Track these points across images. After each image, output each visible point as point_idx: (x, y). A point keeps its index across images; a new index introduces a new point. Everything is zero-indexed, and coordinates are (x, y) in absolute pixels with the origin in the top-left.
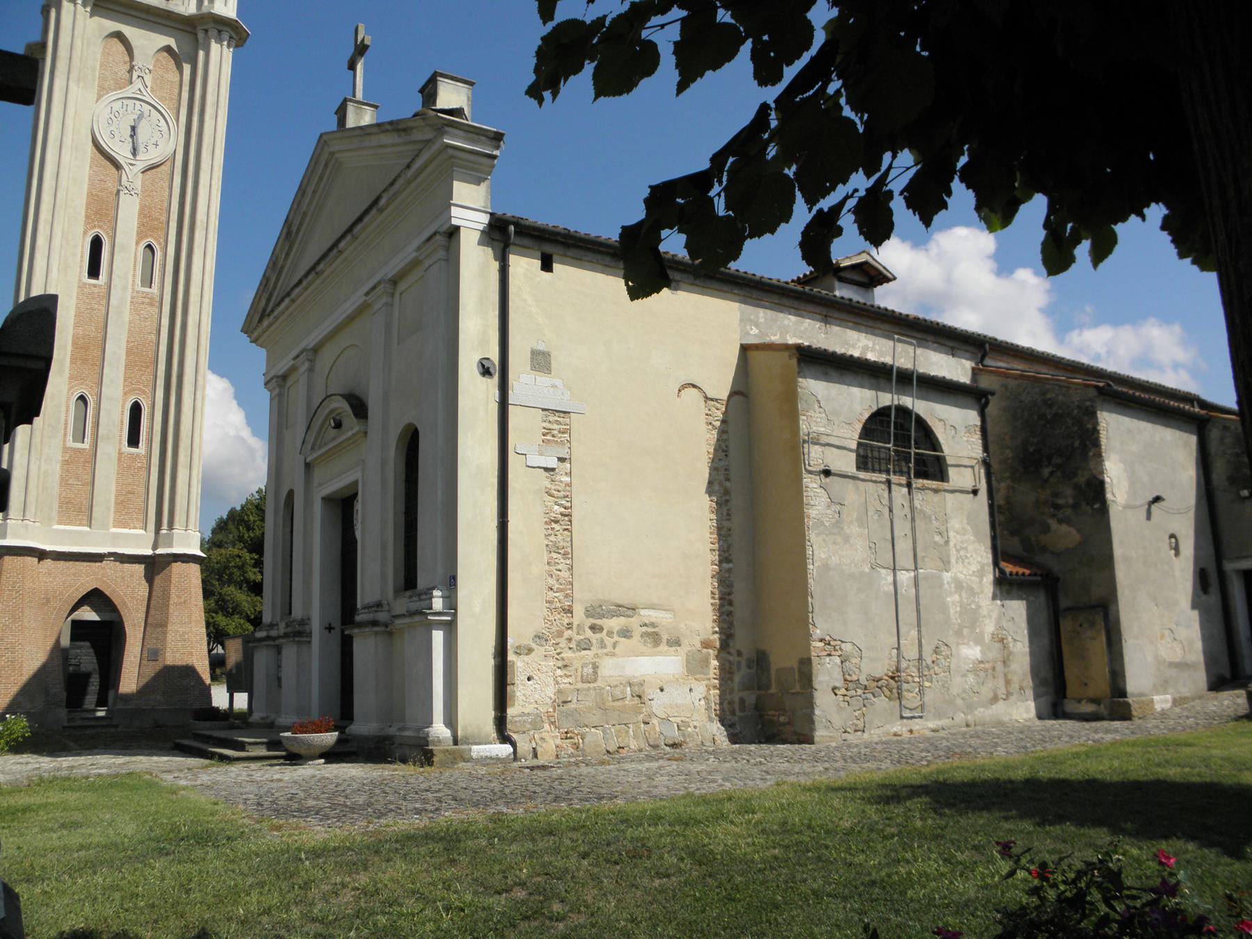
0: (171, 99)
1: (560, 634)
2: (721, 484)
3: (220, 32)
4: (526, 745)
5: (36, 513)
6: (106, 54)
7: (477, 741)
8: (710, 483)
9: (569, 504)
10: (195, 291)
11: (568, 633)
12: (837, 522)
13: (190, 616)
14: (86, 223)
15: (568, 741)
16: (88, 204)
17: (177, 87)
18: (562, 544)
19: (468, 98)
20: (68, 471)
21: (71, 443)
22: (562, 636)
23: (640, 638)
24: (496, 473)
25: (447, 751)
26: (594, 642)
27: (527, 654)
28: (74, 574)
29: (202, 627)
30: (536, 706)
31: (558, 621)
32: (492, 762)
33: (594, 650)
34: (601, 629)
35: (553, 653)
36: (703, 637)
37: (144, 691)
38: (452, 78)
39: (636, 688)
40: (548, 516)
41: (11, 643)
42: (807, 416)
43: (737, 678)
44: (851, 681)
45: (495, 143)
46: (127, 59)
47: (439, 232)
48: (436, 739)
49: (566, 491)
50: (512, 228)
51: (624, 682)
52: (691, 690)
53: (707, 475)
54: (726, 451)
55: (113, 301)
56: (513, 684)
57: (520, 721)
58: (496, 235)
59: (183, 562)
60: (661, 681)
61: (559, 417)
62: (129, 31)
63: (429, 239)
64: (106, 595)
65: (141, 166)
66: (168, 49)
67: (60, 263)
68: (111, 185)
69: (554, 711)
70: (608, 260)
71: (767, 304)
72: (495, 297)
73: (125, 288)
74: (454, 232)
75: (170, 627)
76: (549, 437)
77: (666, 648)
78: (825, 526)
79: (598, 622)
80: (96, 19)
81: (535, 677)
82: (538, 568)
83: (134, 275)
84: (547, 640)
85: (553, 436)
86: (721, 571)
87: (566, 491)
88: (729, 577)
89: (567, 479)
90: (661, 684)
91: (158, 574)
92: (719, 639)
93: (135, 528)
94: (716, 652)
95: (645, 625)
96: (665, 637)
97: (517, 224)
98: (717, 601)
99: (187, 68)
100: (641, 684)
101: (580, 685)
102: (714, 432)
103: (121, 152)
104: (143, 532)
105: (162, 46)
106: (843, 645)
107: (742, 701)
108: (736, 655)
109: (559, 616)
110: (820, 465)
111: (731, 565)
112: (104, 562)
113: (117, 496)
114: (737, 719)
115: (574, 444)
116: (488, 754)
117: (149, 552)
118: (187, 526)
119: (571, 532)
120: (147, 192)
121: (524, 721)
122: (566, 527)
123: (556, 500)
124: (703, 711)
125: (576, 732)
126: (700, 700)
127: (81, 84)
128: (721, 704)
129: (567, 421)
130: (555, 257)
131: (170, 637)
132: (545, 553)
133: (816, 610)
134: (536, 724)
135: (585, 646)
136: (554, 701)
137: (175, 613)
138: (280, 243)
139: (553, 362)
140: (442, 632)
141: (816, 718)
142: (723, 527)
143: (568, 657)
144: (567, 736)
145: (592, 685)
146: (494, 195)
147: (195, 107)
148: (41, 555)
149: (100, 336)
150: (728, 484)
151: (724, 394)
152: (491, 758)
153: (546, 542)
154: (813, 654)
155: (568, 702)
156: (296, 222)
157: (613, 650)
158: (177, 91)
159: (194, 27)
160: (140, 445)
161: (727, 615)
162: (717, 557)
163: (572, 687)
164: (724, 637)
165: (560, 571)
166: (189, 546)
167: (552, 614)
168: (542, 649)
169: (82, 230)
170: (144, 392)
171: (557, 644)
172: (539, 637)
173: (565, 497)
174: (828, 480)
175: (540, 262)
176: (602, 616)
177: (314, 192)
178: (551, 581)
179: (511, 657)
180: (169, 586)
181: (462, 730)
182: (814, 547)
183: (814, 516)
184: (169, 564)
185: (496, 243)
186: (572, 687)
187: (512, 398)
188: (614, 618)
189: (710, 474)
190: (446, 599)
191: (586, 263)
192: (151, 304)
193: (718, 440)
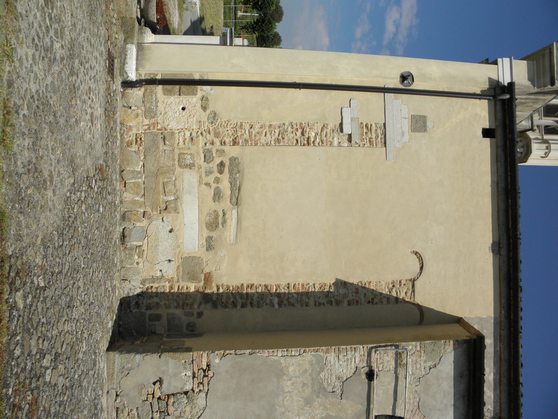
1: (217, 135)
2: (345, 296)
7: (140, 58)
8: (345, 284)
9: (317, 144)
11: (217, 141)
12: (325, 390)
23: (214, 209)
25: (134, 27)
26: (211, 165)
27: (202, 106)
30: (163, 113)
31: (227, 133)
32: (123, 59)
33: (204, 165)
34: (221, 172)
36: (215, 275)
39: (173, 205)
40: (307, 126)
42: (420, 351)
43: (178, 312)
44: (167, 405)
50: (508, 96)
51: (178, 193)
52: (170, 261)
53: (351, 282)
54: (373, 303)
56: (180, 95)
57: (152, 99)
60: (178, 230)
61: (381, 139)
69: (158, 130)
71: (498, 349)
76: (365, 130)
77: (205, 235)
78: (320, 372)
79: (226, 169)
85: (366, 133)
86: (271, 294)
88: (266, 304)
89: (336, 143)
90: (175, 230)
92: (213, 293)
94: (201, 290)
95: (224, 214)
96: (214, 234)
98: (245, 291)
100: (176, 210)
101: (177, 152)
102: (387, 290)
106: (203, 395)
107: (158, 318)
108: (199, 311)
109: (231, 134)
110: (378, 367)
111: (276, 306)
114: (143, 310)
115: (362, 150)
116: (128, 56)
121: (151, 102)
123: (319, 134)
124: (151, 274)
126: (161, 271)
128: (157, 294)
129: (379, 145)
130: (494, 140)
133: (238, 359)
134: (150, 113)
135: (208, 157)
136: (166, 129)
139: (420, 134)
141: (132, 355)
142: (308, 298)
143: (199, 140)
144: (138, 139)
145: (176, 162)
150: (346, 303)
151: (421, 299)
152: (125, 58)
153: (287, 123)
154: (195, 354)
155: (164, 142)
157: (204, 182)
161: (233, 302)
162: (283, 291)
164: (214, 298)
167: (233, 128)
168: (206, 120)
171: (209, 132)
172: (215, 115)
173: (322, 141)
174: (364, 377)
176: (231, 173)
178: (257, 127)
182: (299, 358)
183: (329, 358)
186: (176, 145)
189: (352, 284)
191: (495, 167)
193: (381, 294)
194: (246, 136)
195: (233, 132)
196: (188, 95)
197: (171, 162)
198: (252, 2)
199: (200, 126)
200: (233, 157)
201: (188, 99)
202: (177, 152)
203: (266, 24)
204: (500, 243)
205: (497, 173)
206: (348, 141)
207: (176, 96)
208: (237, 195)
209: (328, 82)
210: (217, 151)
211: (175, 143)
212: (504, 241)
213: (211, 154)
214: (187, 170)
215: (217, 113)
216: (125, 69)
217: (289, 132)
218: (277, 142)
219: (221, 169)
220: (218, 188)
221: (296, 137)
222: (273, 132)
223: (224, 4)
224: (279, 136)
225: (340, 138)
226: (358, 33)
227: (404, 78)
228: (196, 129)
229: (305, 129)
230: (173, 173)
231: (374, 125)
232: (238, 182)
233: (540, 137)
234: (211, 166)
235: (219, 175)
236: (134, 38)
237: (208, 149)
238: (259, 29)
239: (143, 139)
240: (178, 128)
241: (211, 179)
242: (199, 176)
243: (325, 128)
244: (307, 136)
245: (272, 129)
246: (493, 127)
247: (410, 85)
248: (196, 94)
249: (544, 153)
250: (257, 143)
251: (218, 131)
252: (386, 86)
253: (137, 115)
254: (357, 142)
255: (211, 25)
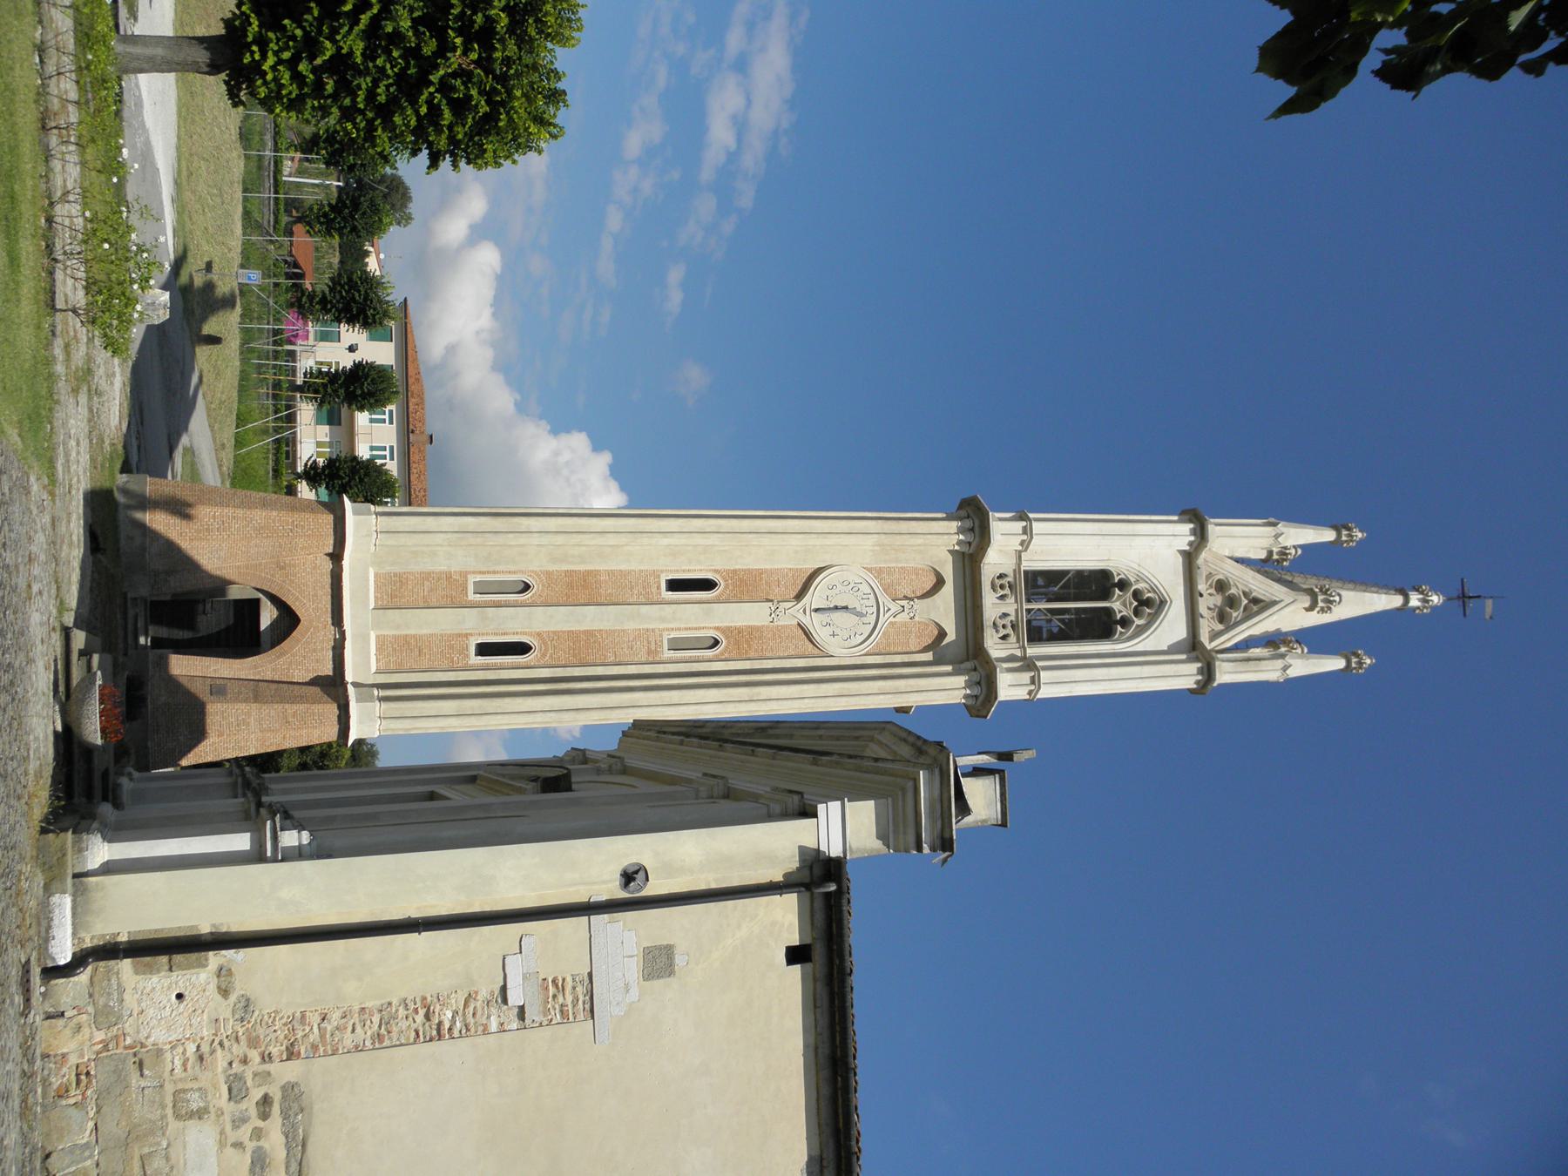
0: (889, 645)
1: (253, 1042)
3: (979, 683)
4: (69, 1000)
5: (387, 546)
6: (916, 571)
7: (79, 910)
9: (456, 1034)
10: (675, 696)
11: (254, 1055)
13: (269, 730)
14: (727, 571)
15: (73, 1078)
16: (750, 571)
17: (904, 650)
18: (395, 1029)
19: (984, 821)
20: (439, 579)
21: (472, 579)
22: (249, 1047)
24: (487, 909)
25: (64, 855)
26: (243, 1105)
27: (219, 987)
28: (316, 595)
29: (257, 749)
30: (135, 1013)
31: (273, 1036)
32: (43, 930)
34: (264, 1116)
35: (223, 1033)
37: (173, 684)
38: (1003, 795)
40: (435, 1000)
41: (230, 527)
45: (938, 842)
46: (918, 594)
47: (802, 797)
48: (84, 845)
49: (476, 1028)
50: (833, 887)
55: (644, 609)
57: (110, 985)
58: (817, 871)
59: (339, 717)
62: (948, 590)
63: (790, 792)
64: (292, 632)
65: (806, 621)
66: (942, 634)
67: (677, 546)
68: (776, 592)
69: (126, 1048)
70: (825, 1050)
72: (735, 882)
73: (662, 619)
74: (808, 812)
75: (254, 706)
76: (552, 990)
80: (950, 558)
81: (182, 1006)
82: (355, 993)
83: (679, 629)
84: (242, 1020)
85: (554, 996)
87: (476, 1028)
89: (494, 1027)
91: (322, 690)
93: (378, 661)
97: (840, 893)
99: (928, 656)
101: (169, 1088)
103: (815, 597)
104: (374, 669)
105: (943, 626)
109: (282, 1037)
112: (333, 628)
113: (414, 636)
115: (547, 1032)
116: (56, 922)
117: (349, 677)
118: (384, 718)
119: (415, 1043)
120: (778, 632)
121: (109, 994)
122: (421, 1034)
123: (460, 1013)
125: (89, 1092)
127: (876, 548)
129: (581, 1016)
130: (809, 966)
131: (242, 706)
132: (378, 1003)
134: (106, 1016)
136: (142, 1045)
137: (272, 711)
138: (751, 724)
139: (661, 981)
140: (248, 848)
144: (82, 1075)
145: (169, 1111)
146: (870, 860)
147: (887, 670)
148: (336, 556)
149: (603, 600)
152: (49, 927)
153: (395, 1002)
155: (141, 1070)
156: (777, 732)
158: (900, 650)
159: (975, 657)
160: (480, 658)
163: (167, 1074)
165: (353, 1031)
166: (360, 722)
167: (285, 1025)
168: (228, 1014)
169: (719, 568)
170: (544, 655)
171: (237, 1040)
172: (247, 1004)
173: (467, 1026)
175: (798, 944)
176: (285, 1115)
177: (820, 737)
178: (335, 1017)
179: (215, 959)
180: (308, 702)
181: (97, 884)
184: (335, 699)
185: (807, 872)
186: (167, 1074)
187: (599, 920)
188: (284, 1138)
190: (297, 852)
192: (649, 652)
194: (315, 1036)
195: (286, 1032)
196: (189, 969)
197: (159, 1112)
198: (325, 148)
199: (218, 1030)
200: (288, 1083)
201: (188, 977)
202: (169, 1088)
203: (364, 213)
204: (822, 1159)
205: (816, 1027)
206: (518, 1018)
207: (163, 974)
208: (300, 1155)
209: (476, 908)
210: (255, 1075)
211: (163, 1072)
212: (830, 1156)
213: (242, 1082)
214: (193, 1125)
215: (253, 998)
216: (51, 950)
217: (400, 1017)
218: (376, 1041)
219: (265, 1111)
220: (260, 1148)
221: (414, 1026)
222: (368, 1022)
223: (245, 190)
224: (380, 1029)
225: (502, 1014)
226: (634, 143)
227: (628, 877)
228: (208, 1035)
229: (432, 1008)
230: (163, 1134)
231: (569, 979)
232: (301, 1131)
233: (1018, 653)
234: (244, 1108)
235: (260, 1124)
236: (66, 880)
237: (236, 1074)
238: (345, 227)
239: (92, 1073)
240: (170, 1039)
241: (244, 1133)
242: (218, 1131)
243: (472, 1000)
244: (437, 1021)
245: (366, 1016)
246: (808, 941)
247: (641, 888)
248: (205, 966)
249: (1027, 691)
250: (337, 1049)
251: (254, 1034)
252: (591, 900)
253: (79, 1028)
254: (536, 1019)
255: (206, 259)
